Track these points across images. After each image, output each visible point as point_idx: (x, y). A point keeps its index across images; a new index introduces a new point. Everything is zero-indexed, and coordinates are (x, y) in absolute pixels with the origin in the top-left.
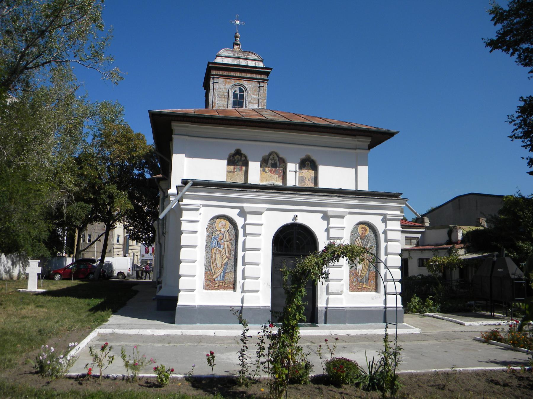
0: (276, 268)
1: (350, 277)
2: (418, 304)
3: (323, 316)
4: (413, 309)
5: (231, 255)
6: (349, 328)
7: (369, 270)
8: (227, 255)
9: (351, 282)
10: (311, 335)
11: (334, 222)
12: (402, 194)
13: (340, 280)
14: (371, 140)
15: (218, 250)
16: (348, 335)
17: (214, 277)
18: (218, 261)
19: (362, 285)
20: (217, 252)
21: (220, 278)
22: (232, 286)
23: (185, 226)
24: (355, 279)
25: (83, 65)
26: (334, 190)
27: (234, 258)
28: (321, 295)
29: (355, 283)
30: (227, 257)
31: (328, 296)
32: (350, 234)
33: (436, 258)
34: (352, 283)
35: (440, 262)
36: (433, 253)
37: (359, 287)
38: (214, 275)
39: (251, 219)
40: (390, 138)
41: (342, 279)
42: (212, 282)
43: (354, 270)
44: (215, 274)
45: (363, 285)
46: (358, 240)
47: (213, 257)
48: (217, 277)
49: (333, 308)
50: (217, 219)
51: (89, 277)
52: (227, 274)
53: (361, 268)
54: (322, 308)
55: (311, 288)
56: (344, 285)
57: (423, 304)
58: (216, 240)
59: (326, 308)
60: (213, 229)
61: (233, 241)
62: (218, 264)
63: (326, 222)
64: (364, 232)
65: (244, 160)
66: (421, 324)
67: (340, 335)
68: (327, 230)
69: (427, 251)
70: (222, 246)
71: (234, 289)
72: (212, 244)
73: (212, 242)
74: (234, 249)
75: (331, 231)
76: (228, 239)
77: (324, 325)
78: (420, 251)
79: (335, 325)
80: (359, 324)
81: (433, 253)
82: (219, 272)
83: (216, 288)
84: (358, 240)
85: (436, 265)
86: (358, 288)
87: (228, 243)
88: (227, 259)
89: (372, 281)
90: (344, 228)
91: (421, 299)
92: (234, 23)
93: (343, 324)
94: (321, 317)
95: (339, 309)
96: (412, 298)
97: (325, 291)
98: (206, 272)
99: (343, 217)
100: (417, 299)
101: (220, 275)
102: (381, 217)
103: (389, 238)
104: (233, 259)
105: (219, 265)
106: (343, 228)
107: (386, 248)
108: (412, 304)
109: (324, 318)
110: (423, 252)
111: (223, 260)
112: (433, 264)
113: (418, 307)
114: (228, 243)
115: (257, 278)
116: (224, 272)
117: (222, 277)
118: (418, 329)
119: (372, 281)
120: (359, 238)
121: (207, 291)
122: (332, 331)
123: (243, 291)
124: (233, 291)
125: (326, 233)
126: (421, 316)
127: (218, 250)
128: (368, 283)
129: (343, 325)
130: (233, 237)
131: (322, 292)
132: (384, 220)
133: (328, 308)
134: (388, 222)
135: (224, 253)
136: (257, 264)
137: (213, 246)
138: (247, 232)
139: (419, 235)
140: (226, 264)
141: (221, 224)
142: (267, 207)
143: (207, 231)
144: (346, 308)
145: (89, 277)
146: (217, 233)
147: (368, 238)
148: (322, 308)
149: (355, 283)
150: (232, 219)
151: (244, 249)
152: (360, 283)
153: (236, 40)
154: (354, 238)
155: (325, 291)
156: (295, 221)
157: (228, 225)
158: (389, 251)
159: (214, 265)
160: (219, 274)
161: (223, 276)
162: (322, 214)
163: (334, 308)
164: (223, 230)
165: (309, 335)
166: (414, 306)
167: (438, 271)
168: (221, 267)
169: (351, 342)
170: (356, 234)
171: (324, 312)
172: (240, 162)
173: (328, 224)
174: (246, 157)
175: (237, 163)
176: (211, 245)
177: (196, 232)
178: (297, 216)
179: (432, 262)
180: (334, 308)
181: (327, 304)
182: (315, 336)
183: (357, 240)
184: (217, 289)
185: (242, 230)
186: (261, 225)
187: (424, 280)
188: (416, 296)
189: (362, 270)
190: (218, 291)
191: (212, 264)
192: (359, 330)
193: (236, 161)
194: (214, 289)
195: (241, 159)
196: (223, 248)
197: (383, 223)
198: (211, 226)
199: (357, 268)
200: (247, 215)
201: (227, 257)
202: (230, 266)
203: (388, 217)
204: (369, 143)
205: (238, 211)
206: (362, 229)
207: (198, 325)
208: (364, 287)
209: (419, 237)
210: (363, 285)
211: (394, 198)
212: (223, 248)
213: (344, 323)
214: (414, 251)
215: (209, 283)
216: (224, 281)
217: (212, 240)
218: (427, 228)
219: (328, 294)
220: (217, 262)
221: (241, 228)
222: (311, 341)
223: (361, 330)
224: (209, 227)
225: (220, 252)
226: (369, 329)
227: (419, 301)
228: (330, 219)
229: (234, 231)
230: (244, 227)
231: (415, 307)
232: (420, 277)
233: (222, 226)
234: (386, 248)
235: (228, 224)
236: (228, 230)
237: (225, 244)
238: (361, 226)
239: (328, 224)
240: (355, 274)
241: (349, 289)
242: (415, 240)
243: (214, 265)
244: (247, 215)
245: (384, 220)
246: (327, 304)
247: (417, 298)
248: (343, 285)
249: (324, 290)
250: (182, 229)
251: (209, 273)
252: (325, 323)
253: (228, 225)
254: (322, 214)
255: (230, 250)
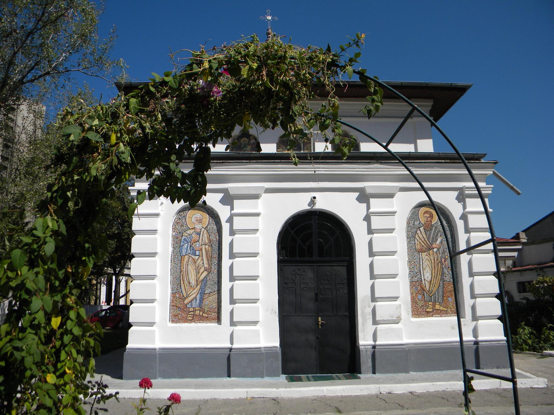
0: (286, 284)
1: (412, 294)
2: (530, 338)
3: (370, 361)
4: (522, 345)
5: (212, 266)
6: (413, 381)
7: (442, 279)
8: (206, 266)
9: (414, 301)
10: (344, 394)
11: (377, 205)
12: (486, 154)
13: (395, 298)
14: (432, 104)
15: (191, 259)
16: (411, 392)
17: (186, 301)
18: (192, 277)
19: (433, 305)
20: (190, 263)
21: (196, 304)
22: (214, 315)
23: (137, 224)
24: (420, 297)
25: (86, 74)
26: (373, 155)
27: (216, 270)
28: (363, 324)
29: (421, 303)
30: (205, 270)
31: (376, 326)
32: (405, 223)
33: (543, 279)
34: (416, 302)
35: (549, 283)
36: (537, 273)
37: (428, 310)
38: (185, 298)
39: (240, 206)
40: (462, 95)
41: (397, 298)
42: (183, 310)
43: (418, 281)
44: (187, 297)
45: (434, 305)
46: (421, 233)
47: (184, 269)
48: (191, 301)
49: (385, 347)
50: (188, 211)
51: (119, 325)
52: (206, 296)
53: (430, 277)
54: (366, 347)
55: (347, 314)
56: (402, 307)
57: (538, 337)
58: (188, 243)
59: (374, 347)
60: (182, 226)
61: (215, 244)
62: (191, 281)
63: (365, 205)
64: (429, 219)
65: (254, 143)
66: (543, 369)
67: (397, 392)
68: (367, 219)
69: (528, 272)
70: (197, 253)
71: (219, 320)
72: (182, 250)
73: (181, 247)
74: (216, 256)
75: (373, 219)
76: (207, 241)
77: (371, 375)
78: (519, 273)
79: (391, 374)
80: (433, 372)
81: (537, 273)
82: (194, 293)
83: (190, 320)
84: (421, 233)
85: (544, 288)
86: (426, 312)
87: (207, 246)
88: (205, 273)
89: (450, 299)
90: (395, 212)
91: (534, 330)
92: (266, 20)
93: (404, 372)
94: (365, 362)
95: (395, 347)
96: (518, 328)
97: (370, 318)
98: (173, 295)
99: (391, 196)
100: (528, 330)
101: (196, 298)
102: (456, 193)
103: (471, 226)
104: (216, 272)
105: (193, 282)
106: (393, 213)
107: (472, 286)
108: (520, 338)
109: (371, 364)
110: (523, 272)
111: (200, 274)
112: (539, 286)
113: (530, 342)
114: (207, 246)
115: (255, 301)
116: (202, 293)
117: (198, 301)
118: (541, 379)
119: (450, 299)
120: (422, 229)
121: (174, 325)
122: (381, 386)
123: (233, 323)
124: (217, 324)
125: (365, 223)
126: (539, 356)
127: (191, 259)
128: (443, 301)
129: (403, 374)
130: (214, 238)
131: (365, 321)
132: (461, 197)
133: (377, 347)
134: (468, 200)
135: (201, 263)
136: (254, 278)
137: (184, 253)
138: (235, 228)
139: (515, 254)
140: (205, 280)
141: (195, 218)
142: (266, 187)
143: (174, 229)
144: (408, 346)
145: (119, 325)
146: (189, 232)
147: (436, 228)
148: (366, 347)
149: (421, 303)
150: (212, 209)
151: (232, 256)
152: (430, 303)
153: (268, 37)
154: (414, 230)
155: (370, 318)
156: (313, 207)
157: (207, 218)
158: (479, 314)
159: (186, 282)
160: (193, 296)
161: (200, 301)
162: (357, 194)
163: (387, 347)
164: (198, 227)
165: (340, 395)
166: (523, 340)
167: (547, 295)
168: (197, 285)
169: (414, 408)
170: (417, 223)
171: (370, 354)
172: (248, 146)
173: (368, 208)
174: (255, 139)
175: (243, 147)
176: (180, 252)
177: (154, 232)
178: (315, 198)
179: (537, 284)
180: (387, 347)
181: (375, 339)
182: (350, 397)
183: (418, 232)
184: (191, 321)
185: (228, 224)
186: (258, 215)
187: (531, 307)
188: (526, 325)
189: (431, 281)
190: (193, 325)
191: (182, 282)
192: (431, 383)
193: (242, 146)
194: (186, 320)
195: (249, 142)
196: (199, 255)
197: (459, 202)
198: (178, 221)
199: (423, 278)
200: (234, 200)
201: (205, 270)
202: (211, 283)
203: (466, 192)
204: (430, 108)
205: (221, 195)
206: (426, 215)
207: (412, 373)
208: (437, 310)
209: (515, 256)
210: (434, 305)
211: (474, 161)
212: (199, 255)
213: (406, 370)
214: (510, 274)
215: (178, 312)
216: (201, 309)
217: (182, 244)
218: (523, 244)
219: (375, 322)
220: (190, 277)
221: (226, 222)
222: (337, 408)
223: (434, 383)
224: (176, 224)
225: (195, 262)
226: (449, 380)
227: (531, 333)
228: (371, 199)
229: (215, 227)
230: (230, 220)
231: (525, 342)
232: (524, 302)
233: (197, 220)
234: (472, 286)
235: (206, 218)
236: (207, 227)
237: (201, 249)
238: (423, 209)
239: (368, 208)
240: (419, 288)
241: (411, 313)
242: (510, 260)
243: (186, 282)
244: (234, 200)
245: (461, 197)
246: (375, 339)
247: (526, 327)
248: (400, 306)
249: (368, 317)
250: (134, 228)
251: (177, 295)
252: (374, 373)
253: (207, 218)
254: (357, 194)
255: (210, 259)
